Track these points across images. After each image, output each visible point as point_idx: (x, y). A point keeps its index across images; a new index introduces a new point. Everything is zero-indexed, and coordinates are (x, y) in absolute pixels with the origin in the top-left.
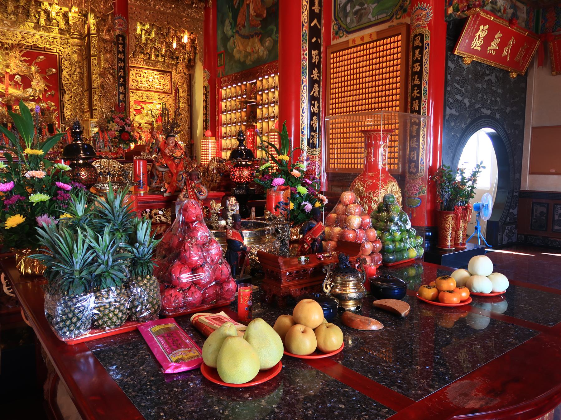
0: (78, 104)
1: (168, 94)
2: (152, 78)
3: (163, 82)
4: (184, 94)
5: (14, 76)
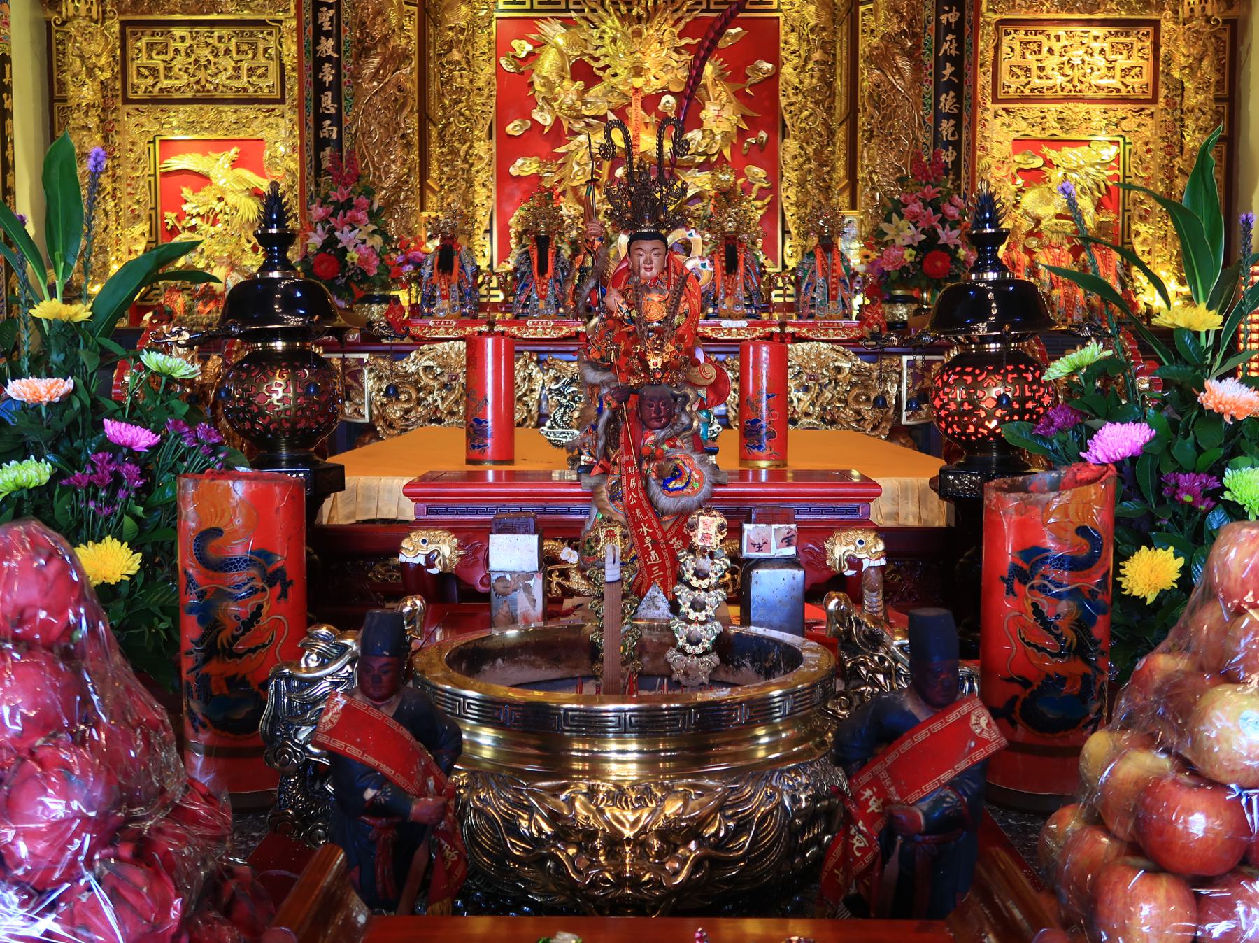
0: (813, 165)
1: (1139, 103)
2: (1081, 52)
3: (1122, 61)
4: (1201, 98)
5: (657, 97)
